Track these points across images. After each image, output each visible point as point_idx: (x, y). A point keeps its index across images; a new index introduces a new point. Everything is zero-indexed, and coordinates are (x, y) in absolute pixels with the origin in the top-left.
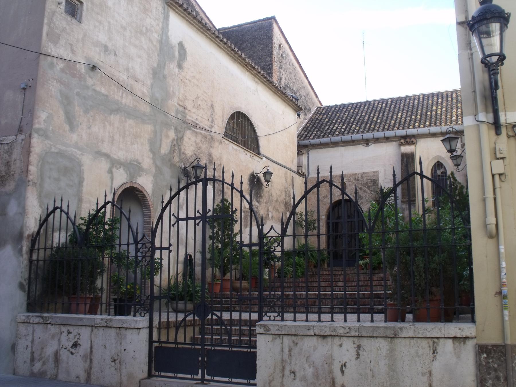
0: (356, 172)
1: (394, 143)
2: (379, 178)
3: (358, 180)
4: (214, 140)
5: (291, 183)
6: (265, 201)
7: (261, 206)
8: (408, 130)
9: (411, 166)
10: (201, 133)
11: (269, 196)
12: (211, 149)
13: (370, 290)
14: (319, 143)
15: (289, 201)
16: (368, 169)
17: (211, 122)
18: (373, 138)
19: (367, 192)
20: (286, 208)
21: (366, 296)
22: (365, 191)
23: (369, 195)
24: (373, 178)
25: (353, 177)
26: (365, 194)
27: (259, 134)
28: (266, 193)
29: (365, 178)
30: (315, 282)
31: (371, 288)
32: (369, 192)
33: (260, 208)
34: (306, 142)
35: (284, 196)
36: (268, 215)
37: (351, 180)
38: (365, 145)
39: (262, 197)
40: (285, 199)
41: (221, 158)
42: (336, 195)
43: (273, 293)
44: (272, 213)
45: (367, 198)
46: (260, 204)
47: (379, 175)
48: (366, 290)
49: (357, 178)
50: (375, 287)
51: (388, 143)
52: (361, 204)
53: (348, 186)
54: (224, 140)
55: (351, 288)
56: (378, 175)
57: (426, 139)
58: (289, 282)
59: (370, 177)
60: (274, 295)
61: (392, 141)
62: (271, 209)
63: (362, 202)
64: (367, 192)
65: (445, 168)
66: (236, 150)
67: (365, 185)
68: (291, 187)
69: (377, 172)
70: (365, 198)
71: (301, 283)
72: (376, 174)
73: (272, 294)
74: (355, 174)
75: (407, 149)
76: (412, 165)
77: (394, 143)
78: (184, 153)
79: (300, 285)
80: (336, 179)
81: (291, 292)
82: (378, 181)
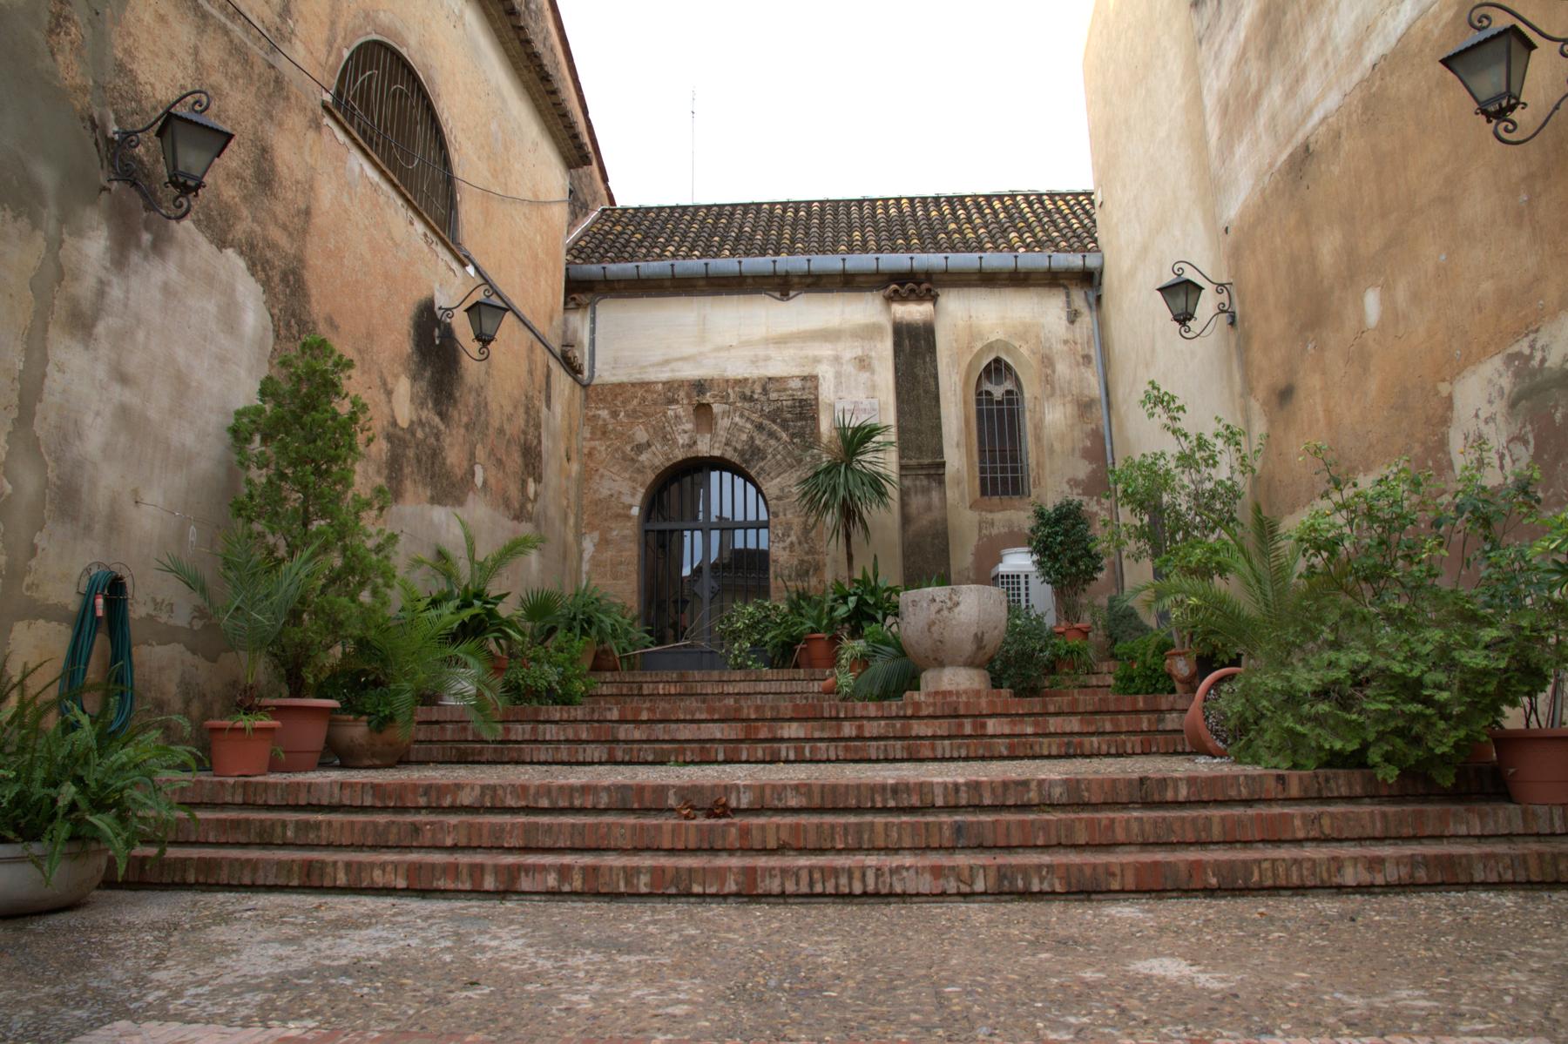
0: (746, 375)
3: (751, 399)
4: (287, 98)
5: (544, 386)
6: (465, 419)
7: (451, 435)
9: (924, 362)
10: (227, 32)
11: (477, 406)
12: (267, 125)
15: (535, 442)
16: (782, 364)
17: (280, 16)
19: (778, 439)
20: (526, 466)
22: (772, 435)
23: (784, 448)
25: (737, 389)
26: (772, 442)
27: (459, 171)
28: (470, 392)
29: (774, 396)
30: (684, 721)
32: (784, 436)
33: (448, 440)
34: (594, 269)
35: (522, 423)
36: (473, 475)
39: (456, 401)
40: (525, 433)
41: (311, 188)
42: (681, 442)
44: (485, 470)
45: (779, 457)
46: (447, 426)
50: (947, 742)
52: (759, 474)
54: (327, 121)
62: (480, 453)
63: (762, 469)
64: (778, 439)
65: (1017, 380)
66: (375, 188)
67: (774, 416)
68: (543, 398)
70: (774, 456)
74: (742, 382)
75: (914, 312)
78: (121, 68)
79: (622, 736)
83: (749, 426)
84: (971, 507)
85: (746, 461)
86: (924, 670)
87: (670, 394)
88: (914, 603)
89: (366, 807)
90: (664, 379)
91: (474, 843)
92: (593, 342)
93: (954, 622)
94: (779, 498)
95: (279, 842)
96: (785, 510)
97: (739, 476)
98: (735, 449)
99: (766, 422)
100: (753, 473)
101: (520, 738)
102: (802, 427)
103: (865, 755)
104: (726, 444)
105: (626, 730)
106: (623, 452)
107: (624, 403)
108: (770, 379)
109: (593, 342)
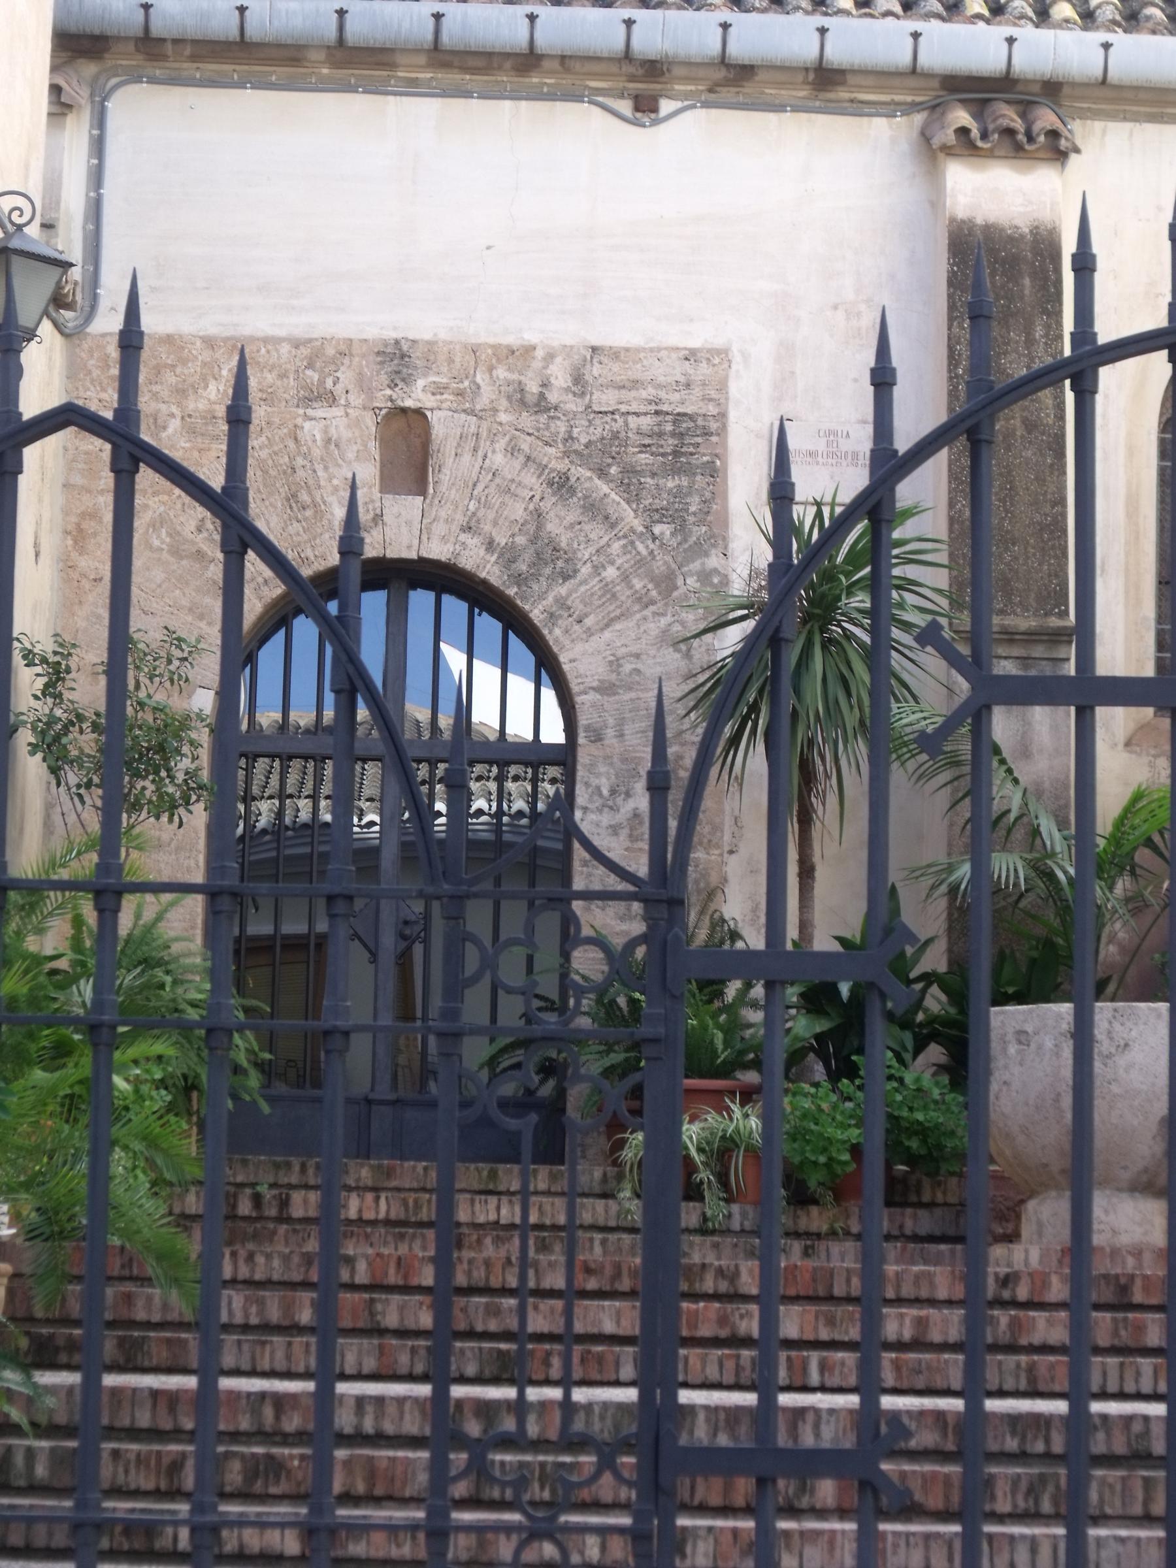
0: (531, 337)
1: (879, 127)
2: (733, 415)
3: (541, 406)
8: (1027, 33)
13: (1062, 1385)
14: (233, 33)
18: (627, 55)
19: (610, 523)
21: (533, 1429)
22: (594, 509)
24: (673, 402)
25: (501, 373)
26: (596, 532)
29: (606, 399)
31: (326, 1354)
32: (631, 518)
37: (483, 401)
38: (625, 107)
43: (555, 1393)
45: (611, 573)
47: (734, 388)
48: (1032, 1379)
49: (533, 388)
50: (1113, 1361)
51: (822, 120)
53: (449, 448)
55: (897, 1366)
56: (723, 387)
57: (1151, 129)
58: (249, 1283)
59: (649, 392)
60: (520, 1407)
61: (858, 109)
64: (610, 523)
66: (1031, 1012)
69: (719, 356)
70: (597, 569)
71: (396, 1298)
72: (704, 369)
73: (544, 1406)
74: (518, 355)
76: (1039, 332)
77: (880, 123)
79: (391, 1320)
80: (346, 376)
81: (289, 1375)
82: (723, 431)
83: (530, 479)
84: (1128, 744)
85: (519, 580)
86: (1032, 1194)
87: (313, 376)
88: (1022, 1036)
89: (141, 1430)
90: (299, 333)
91: (379, 1491)
92: (95, 210)
93: (1115, 1088)
94: (606, 689)
95: (22, 1483)
96: (621, 723)
97: (451, 592)
98: (490, 545)
99: (580, 472)
100: (536, 615)
101: (156, 1318)
102: (678, 493)
103: (940, 1384)
104: (467, 529)
105: (402, 1308)
106: (174, 534)
107: (181, 392)
108: (594, 349)
109: (95, 210)
